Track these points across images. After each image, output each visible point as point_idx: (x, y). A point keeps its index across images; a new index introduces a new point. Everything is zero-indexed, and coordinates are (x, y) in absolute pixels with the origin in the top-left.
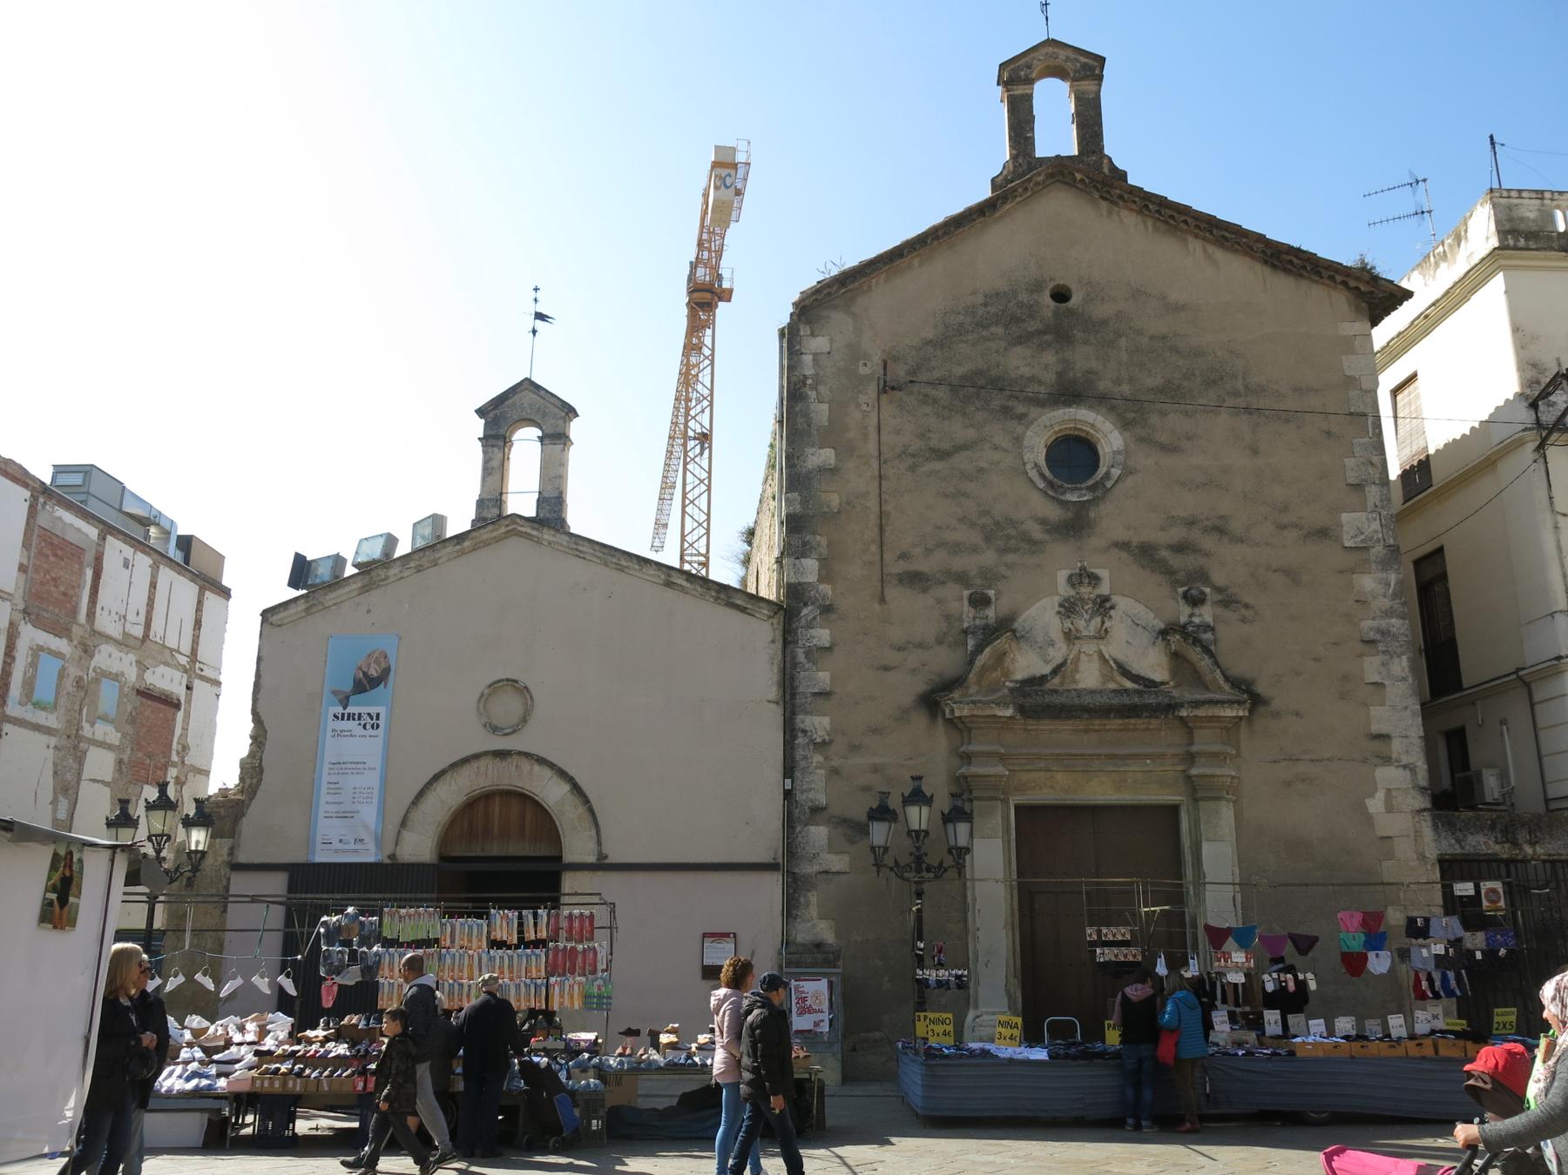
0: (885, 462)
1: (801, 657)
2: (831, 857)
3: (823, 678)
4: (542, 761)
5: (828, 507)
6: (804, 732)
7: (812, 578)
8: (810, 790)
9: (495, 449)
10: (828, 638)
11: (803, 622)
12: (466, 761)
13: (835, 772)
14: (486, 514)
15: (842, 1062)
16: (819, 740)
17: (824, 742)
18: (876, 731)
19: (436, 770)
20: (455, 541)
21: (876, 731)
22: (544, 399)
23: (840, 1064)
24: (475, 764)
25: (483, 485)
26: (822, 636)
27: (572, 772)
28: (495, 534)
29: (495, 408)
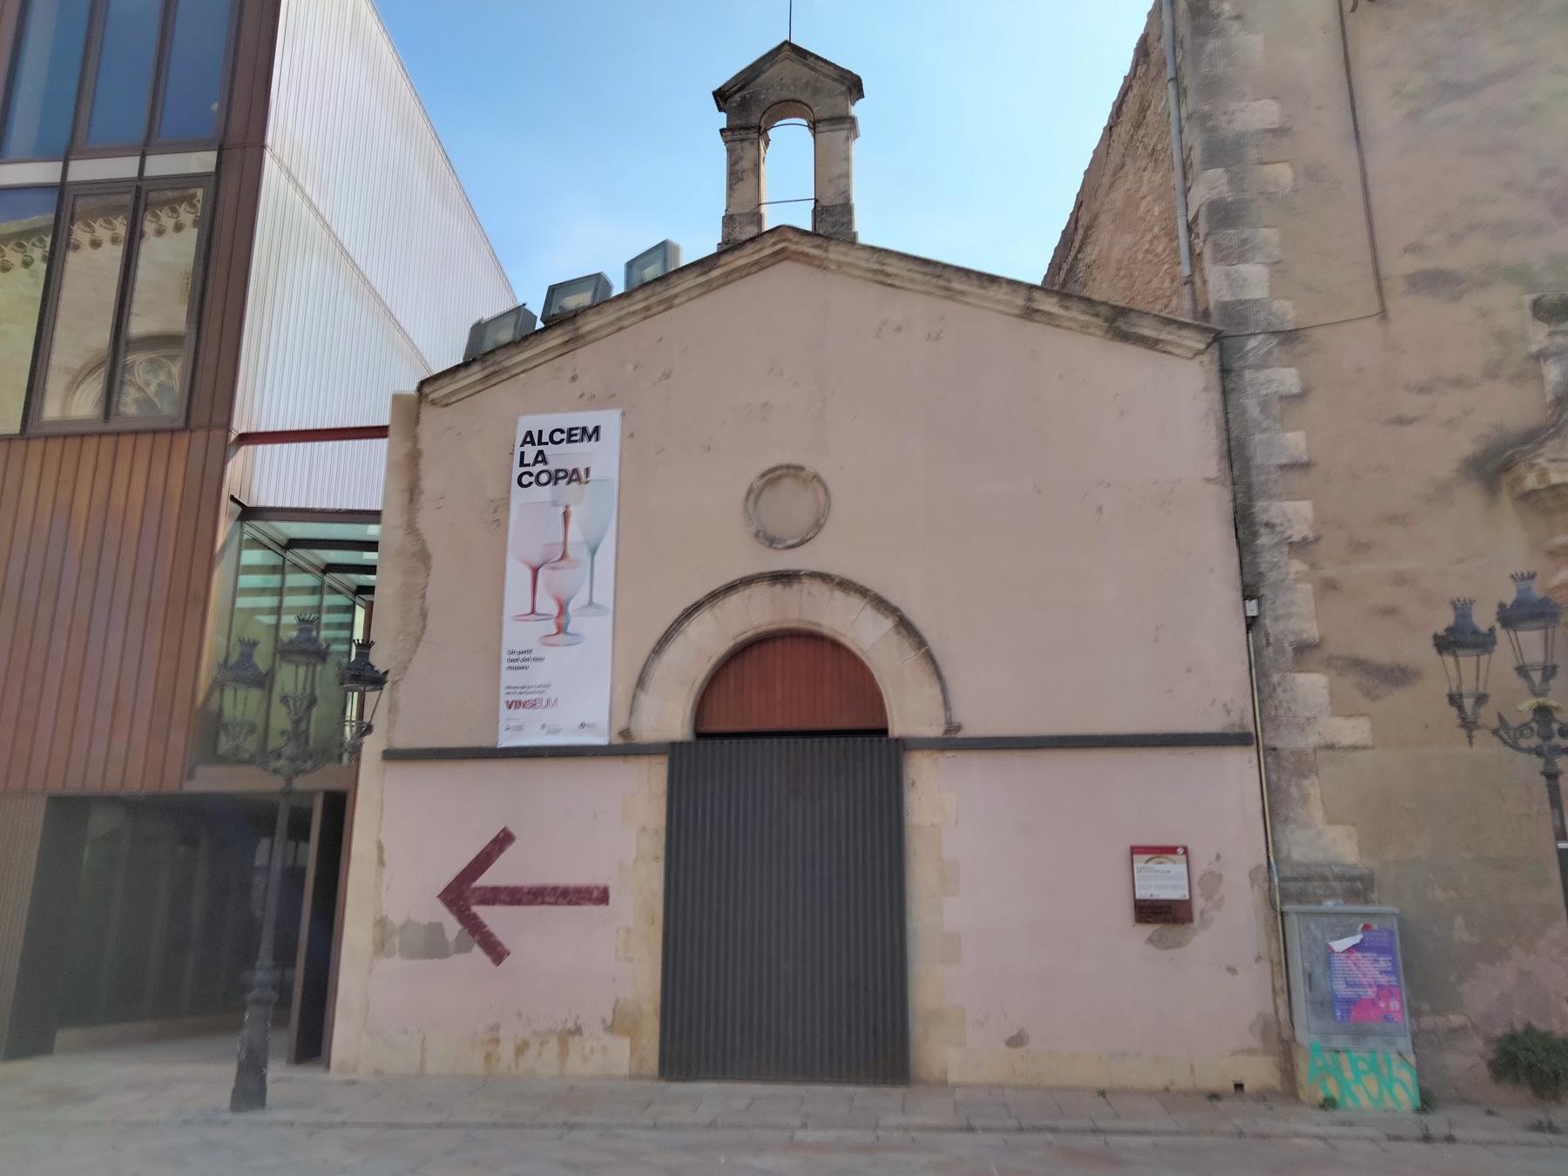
2: (1338, 722)
3: (1295, 442)
4: (845, 585)
8: (1288, 616)
9: (746, 144)
11: (1251, 360)
12: (731, 588)
13: (1329, 587)
15: (1417, 1069)
16: (1296, 538)
17: (1305, 543)
18: (1393, 519)
19: (689, 603)
20: (698, 270)
21: (1393, 519)
22: (813, 69)
23: (1414, 1071)
25: (730, 196)
26: (1286, 378)
27: (894, 598)
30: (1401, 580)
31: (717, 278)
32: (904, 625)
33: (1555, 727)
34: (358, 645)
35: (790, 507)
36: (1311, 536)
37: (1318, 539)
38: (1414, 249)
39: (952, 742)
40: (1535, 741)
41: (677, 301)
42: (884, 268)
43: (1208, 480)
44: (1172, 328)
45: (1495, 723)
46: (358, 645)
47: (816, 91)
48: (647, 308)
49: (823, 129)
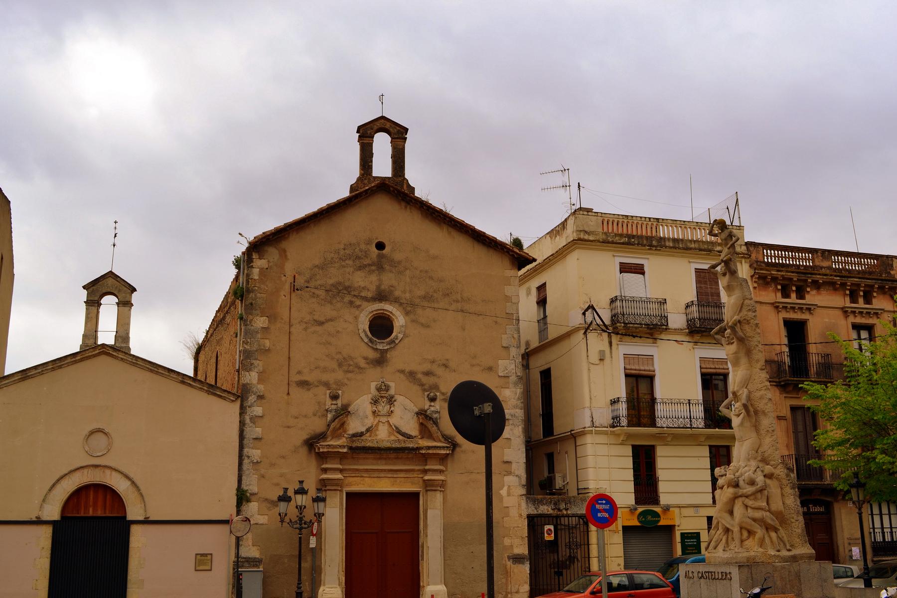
0: (292, 326)
1: (248, 421)
3: (258, 431)
5: (264, 346)
6: (248, 457)
7: (255, 381)
8: (250, 484)
9: (93, 308)
10: (261, 412)
14: (87, 342)
16: (255, 461)
17: (257, 462)
18: (283, 457)
21: (283, 457)
24: (82, 471)
26: (258, 410)
27: (131, 475)
28: (94, 353)
29: (93, 286)
30: (281, 476)
31: (79, 359)
32: (133, 483)
33: (303, 522)
34: (863, 451)
35: (99, 441)
36: (259, 460)
37: (261, 462)
38: (299, 373)
39: (147, 522)
40: (298, 526)
41: (62, 367)
42: (137, 362)
43: (445, 370)
44: (226, 393)
45: (288, 521)
46: (863, 451)
47: (120, 291)
48: (53, 368)
49: (121, 306)
